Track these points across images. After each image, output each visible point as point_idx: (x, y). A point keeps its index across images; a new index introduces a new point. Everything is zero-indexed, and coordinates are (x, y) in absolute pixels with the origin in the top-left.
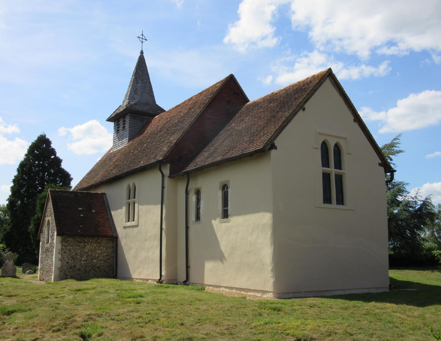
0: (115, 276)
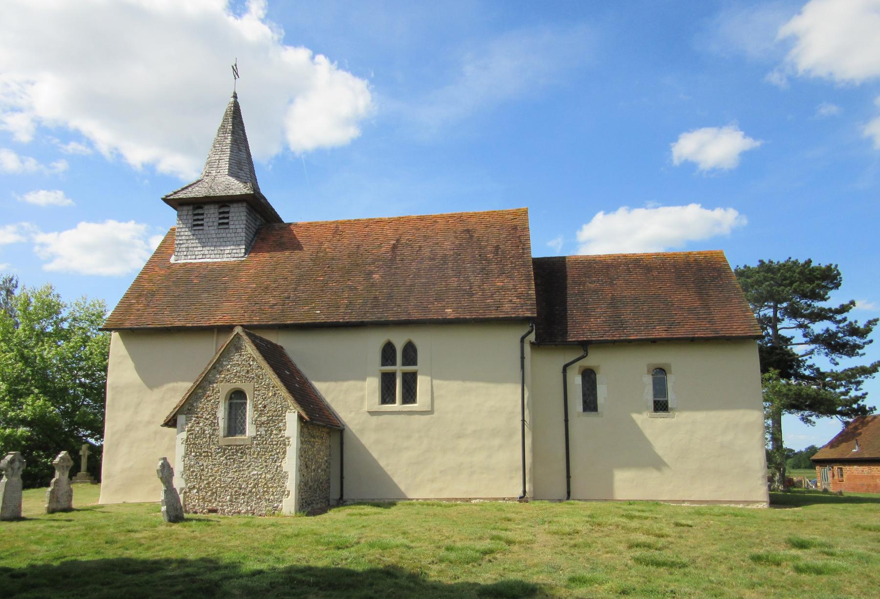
0: (341, 502)
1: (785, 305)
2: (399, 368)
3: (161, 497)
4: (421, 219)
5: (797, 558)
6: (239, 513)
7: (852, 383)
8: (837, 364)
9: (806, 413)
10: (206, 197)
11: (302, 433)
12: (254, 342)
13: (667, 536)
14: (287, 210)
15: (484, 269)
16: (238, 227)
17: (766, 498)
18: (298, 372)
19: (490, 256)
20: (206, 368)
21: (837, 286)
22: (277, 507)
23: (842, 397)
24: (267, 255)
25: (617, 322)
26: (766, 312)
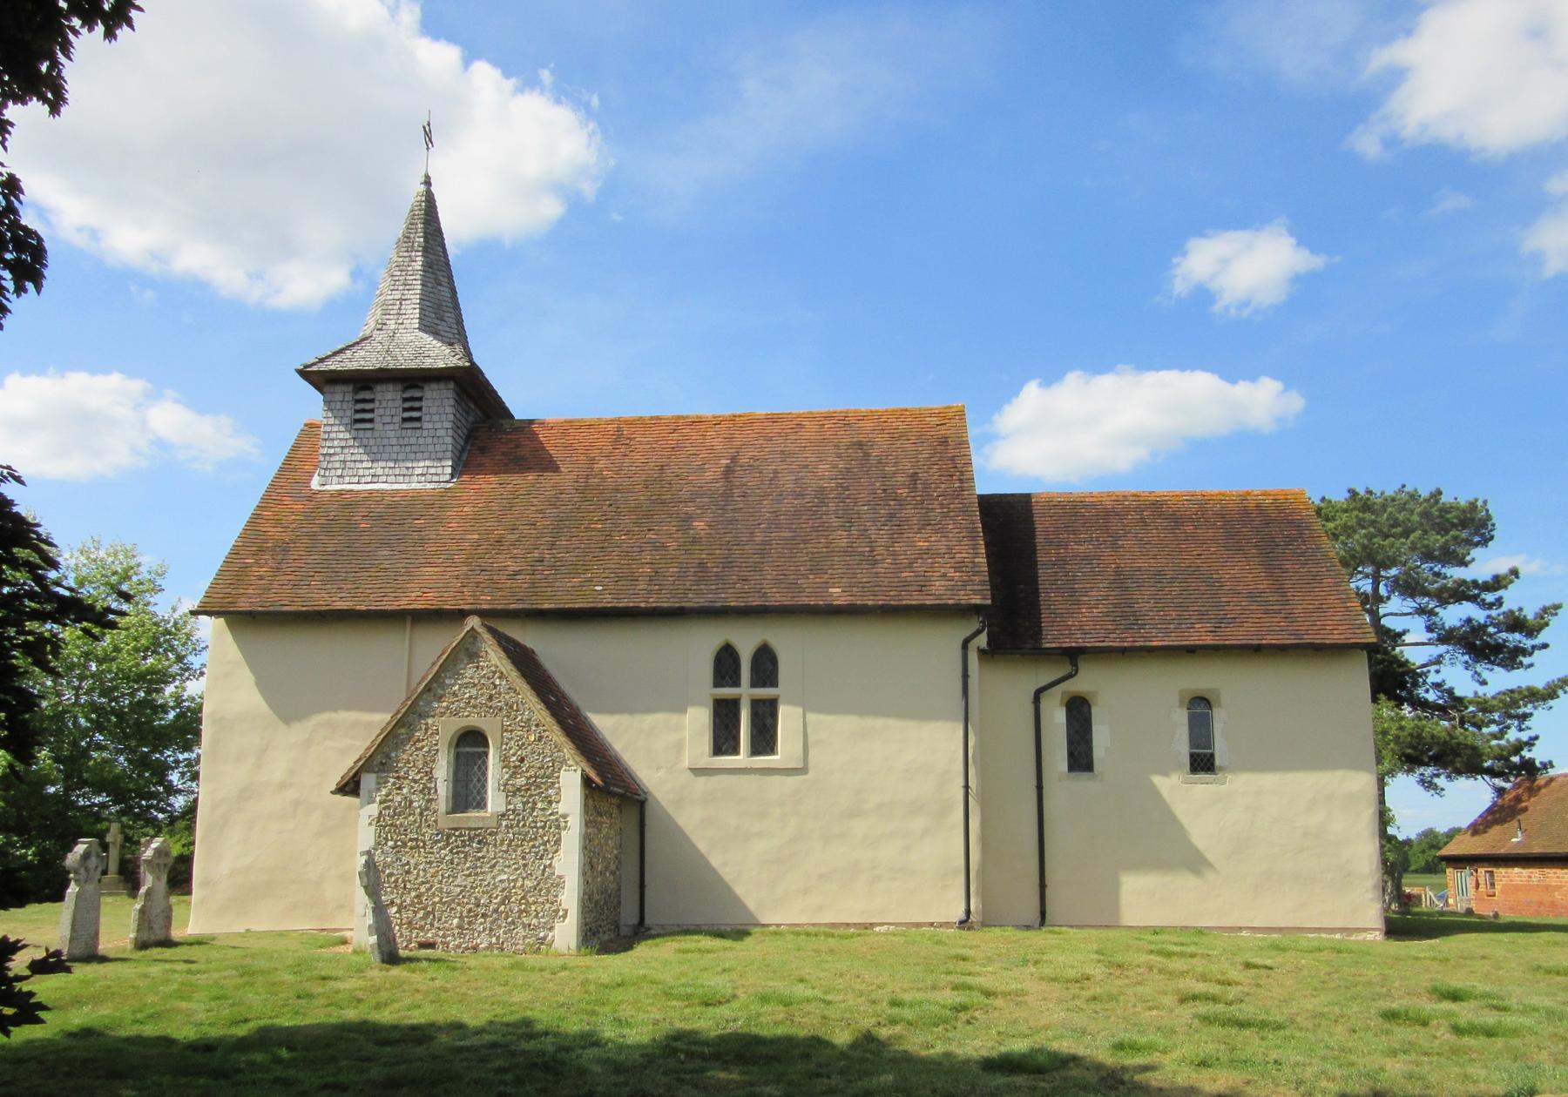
1: (1393, 572)
2: (745, 692)
4: (773, 419)
5: (1449, 1014)
6: (475, 948)
7: (1510, 717)
8: (1484, 683)
9: (1429, 771)
10: (380, 370)
13: (1237, 983)
14: (522, 395)
15: (892, 516)
16: (438, 425)
17: (1379, 923)
18: (564, 696)
19: (903, 492)
21: (1485, 541)
22: (544, 938)
23: (1494, 742)
24: (493, 478)
25: (1128, 616)
26: (1360, 583)
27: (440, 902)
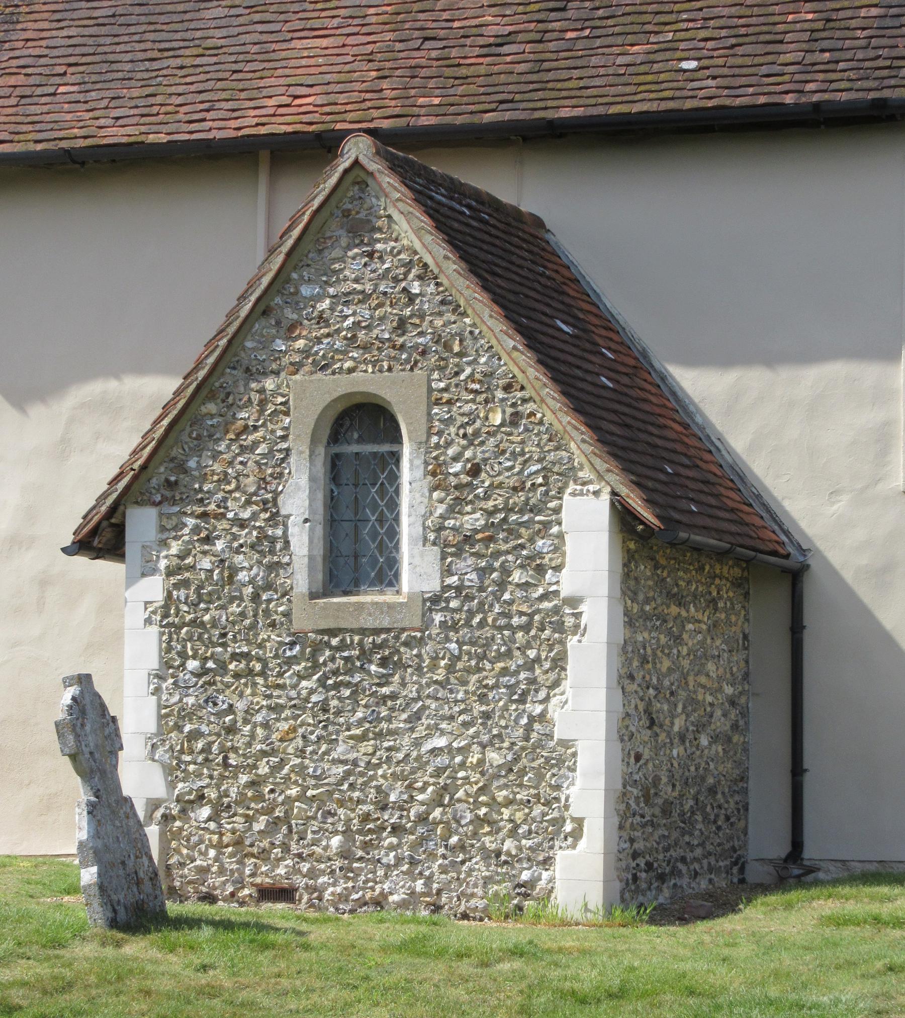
0: (795, 870)
3: (80, 829)
6: (379, 903)
11: (628, 582)
12: (422, 199)
20: (232, 315)
22: (531, 884)
27: (302, 797)
